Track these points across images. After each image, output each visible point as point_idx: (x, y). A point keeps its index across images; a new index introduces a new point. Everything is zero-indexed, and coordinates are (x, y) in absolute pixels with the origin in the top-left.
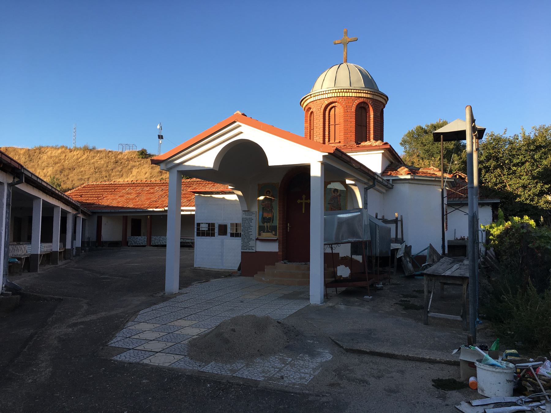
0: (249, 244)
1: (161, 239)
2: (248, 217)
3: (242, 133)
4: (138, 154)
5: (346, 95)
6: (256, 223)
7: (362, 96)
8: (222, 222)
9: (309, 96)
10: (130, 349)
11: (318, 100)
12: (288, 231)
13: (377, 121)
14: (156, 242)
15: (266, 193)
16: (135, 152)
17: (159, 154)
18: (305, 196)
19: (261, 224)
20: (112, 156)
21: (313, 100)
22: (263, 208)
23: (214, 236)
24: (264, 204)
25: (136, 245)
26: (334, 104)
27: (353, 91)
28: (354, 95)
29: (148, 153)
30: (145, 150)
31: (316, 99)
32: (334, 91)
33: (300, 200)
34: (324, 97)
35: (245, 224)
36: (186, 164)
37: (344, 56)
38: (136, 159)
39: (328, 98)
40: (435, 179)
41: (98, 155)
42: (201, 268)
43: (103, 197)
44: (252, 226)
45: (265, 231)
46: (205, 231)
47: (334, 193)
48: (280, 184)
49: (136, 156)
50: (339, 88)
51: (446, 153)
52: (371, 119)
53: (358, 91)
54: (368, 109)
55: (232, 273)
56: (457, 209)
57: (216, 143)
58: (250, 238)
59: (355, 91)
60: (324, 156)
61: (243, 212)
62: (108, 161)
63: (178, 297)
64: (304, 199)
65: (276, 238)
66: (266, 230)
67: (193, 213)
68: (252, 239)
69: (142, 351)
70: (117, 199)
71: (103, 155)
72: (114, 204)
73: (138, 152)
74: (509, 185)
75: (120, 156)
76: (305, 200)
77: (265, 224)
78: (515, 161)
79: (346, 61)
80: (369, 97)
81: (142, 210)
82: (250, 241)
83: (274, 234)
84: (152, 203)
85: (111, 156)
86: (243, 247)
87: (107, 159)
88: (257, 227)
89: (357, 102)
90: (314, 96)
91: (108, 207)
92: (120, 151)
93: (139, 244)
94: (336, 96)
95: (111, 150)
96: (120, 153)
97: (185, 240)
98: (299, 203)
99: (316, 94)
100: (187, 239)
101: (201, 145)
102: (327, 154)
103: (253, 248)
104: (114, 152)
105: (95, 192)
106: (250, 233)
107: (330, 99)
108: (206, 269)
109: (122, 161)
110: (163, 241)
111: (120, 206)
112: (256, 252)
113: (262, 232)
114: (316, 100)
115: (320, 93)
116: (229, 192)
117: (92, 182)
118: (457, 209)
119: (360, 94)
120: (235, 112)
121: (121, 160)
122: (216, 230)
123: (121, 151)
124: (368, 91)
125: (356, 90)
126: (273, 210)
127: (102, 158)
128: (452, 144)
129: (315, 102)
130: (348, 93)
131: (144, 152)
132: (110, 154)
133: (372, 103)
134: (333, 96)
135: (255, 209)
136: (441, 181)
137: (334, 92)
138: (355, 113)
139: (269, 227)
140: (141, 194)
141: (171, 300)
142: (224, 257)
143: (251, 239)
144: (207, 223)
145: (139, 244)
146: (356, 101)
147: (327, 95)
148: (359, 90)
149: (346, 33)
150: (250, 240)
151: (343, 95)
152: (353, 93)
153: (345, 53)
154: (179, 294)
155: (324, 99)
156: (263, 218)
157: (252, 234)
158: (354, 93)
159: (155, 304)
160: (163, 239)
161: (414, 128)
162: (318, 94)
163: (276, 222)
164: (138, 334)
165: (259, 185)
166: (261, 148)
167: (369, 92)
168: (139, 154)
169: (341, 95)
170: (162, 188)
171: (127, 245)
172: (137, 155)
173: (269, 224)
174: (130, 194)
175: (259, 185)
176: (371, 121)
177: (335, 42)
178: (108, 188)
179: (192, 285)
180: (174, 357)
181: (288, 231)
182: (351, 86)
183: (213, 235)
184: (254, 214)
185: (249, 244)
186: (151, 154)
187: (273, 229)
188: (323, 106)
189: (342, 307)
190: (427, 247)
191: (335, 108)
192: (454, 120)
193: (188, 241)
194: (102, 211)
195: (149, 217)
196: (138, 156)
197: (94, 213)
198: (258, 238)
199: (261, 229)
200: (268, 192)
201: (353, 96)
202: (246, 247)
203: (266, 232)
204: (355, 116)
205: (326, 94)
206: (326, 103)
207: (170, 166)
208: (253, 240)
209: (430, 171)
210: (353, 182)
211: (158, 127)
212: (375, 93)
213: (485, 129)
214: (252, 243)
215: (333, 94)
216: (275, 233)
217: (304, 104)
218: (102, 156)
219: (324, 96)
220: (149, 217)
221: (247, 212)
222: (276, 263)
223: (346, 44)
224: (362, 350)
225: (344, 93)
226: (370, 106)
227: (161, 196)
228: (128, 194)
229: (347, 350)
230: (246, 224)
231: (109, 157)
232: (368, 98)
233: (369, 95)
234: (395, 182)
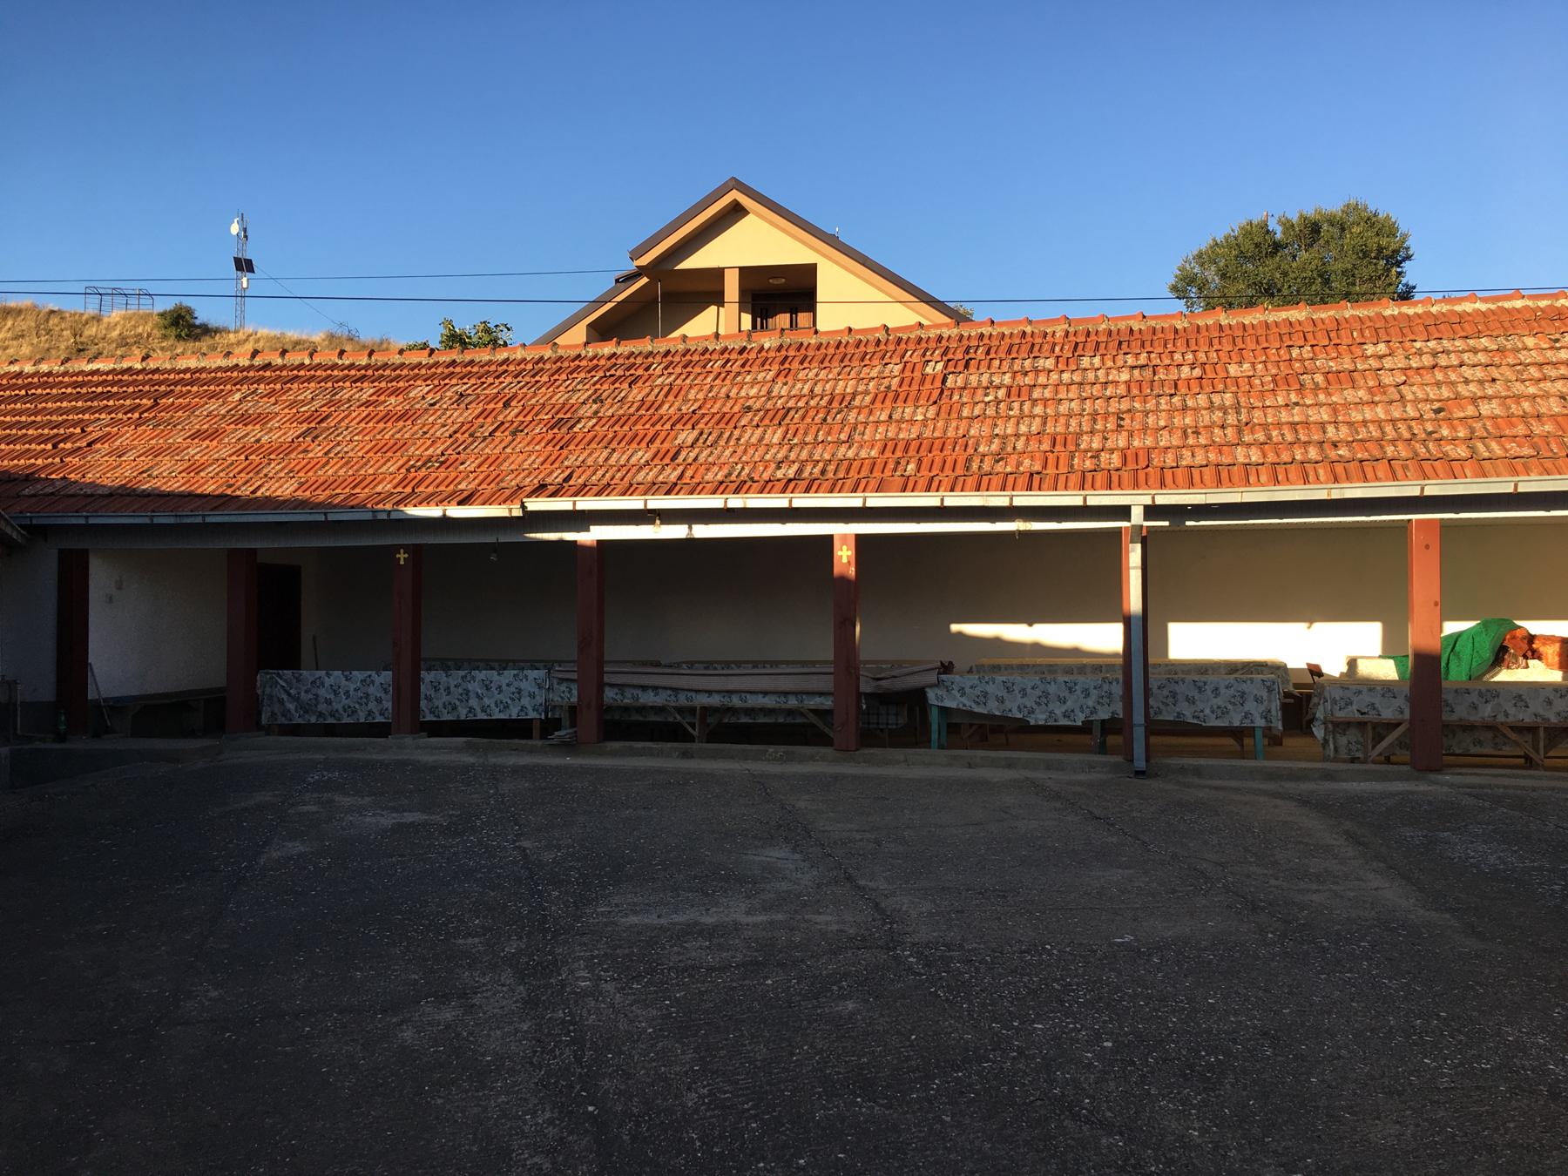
1: (475, 687)
4: (162, 322)
14: (439, 703)
16: (151, 315)
17: (238, 324)
20: (62, 330)
25: (313, 720)
29: (198, 322)
30: (190, 311)
38: (156, 341)
41: (9, 323)
43: (90, 438)
49: (155, 331)
62: (47, 346)
70: (179, 450)
71: (23, 324)
72: (168, 477)
73: (162, 315)
75: (94, 329)
81: (369, 516)
84: (423, 472)
85: (57, 329)
87: (43, 339)
91: (125, 496)
92: (92, 310)
93: (305, 708)
95: (56, 309)
96: (93, 318)
100: (644, 688)
104: (68, 315)
105: (36, 414)
109: (100, 345)
110: (486, 701)
111: (209, 488)
117: (11, 363)
121: (96, 344)
123: (97, 312)
127: (23, 336)
131: (184, 317)
132: (54, 321)
140: (331, 422)
145: (332, 715)
161: (1233, 231)
168: (166, 323)
170: (462, 389)
171: (258, 726)
172: (156, 326)
174: (261, 419)
178: (115, 389)
186: (210, 326)
193: (649, 699)
194: (91, 521)
195: (402, 556)
196: (163, 332)
197: (39, 532)
211: (235, 229)
218: (24, 327)
220: (402, 556)
227: (469, 429)
228: (245, 420)
231: (51, 330)
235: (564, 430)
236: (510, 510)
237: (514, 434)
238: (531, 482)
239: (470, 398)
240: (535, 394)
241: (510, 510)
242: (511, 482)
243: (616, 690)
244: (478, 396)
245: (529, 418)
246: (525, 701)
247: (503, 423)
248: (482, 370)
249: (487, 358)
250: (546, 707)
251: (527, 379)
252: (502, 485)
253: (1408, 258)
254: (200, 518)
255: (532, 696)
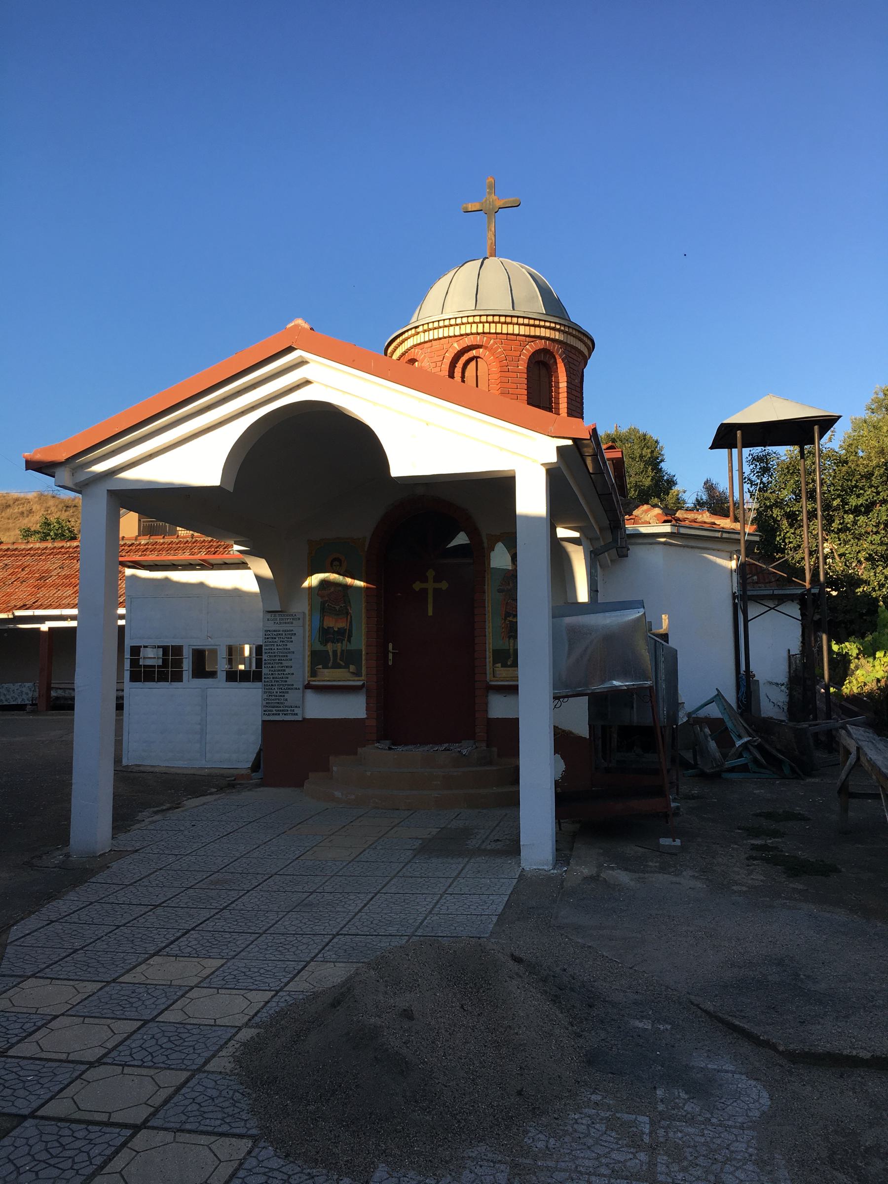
2: (281, 629)
3: (308, 382)
5: (505, 331)
6: (304, 643)
7: (543, 334)
8: (198, 644)
9: (413, 331)
10: (24, 1118)
11: (436, 340)
12: (390, 663)
13: (574, 398)
18: (434, 573)
19: (319, 647)
21: (422, 341)
22: (323, 604)
26: (474, 351)
27: (521, 321)
28: (523, 330)
31: (431, 338)
32: (477, 319)
34: (451, 334)
36: (125, 475)
37: (489, 242)
39: (462, 337)
40: (722, 535)
42: (142, 769)
46: (154, 666)
48: (367, 544)
50: (488, 313)
51: (638, 495)
52: (561, 391)
53: (532, 321)
54: (555, 367)
55: (235, 780)
56: (773, 608)
57: (180, 435)
58: (288, 685)
59: (526, 321)
60: (560, 450)
61: (269, 616)
63: (115, 866)
65: (360, 683)
66: (331, 661)
67: (74, 624)
69: (73, 1126)
74: (839, 555)
77: (330, 647)
78: (853, 501)
79: (493, 254)
80: (557, 337)
82: (288, 693)
83: (353, 673)
86: (267, 707)
88: (307, 653)
89: (530, 348)
90: (425, 331)
94: (480, 330)
97: (67, 691)
99: (431, 326)
101: (185, 414)
102: (569, 442)
103: (296, 710)
106: (288, 671)
107: (466, 339)
108: (157, 770)
110: (8, 697)
112: (304, 719)
113: (320, 666)
114: (430, 341)
115: (441, 324)
116: (221, 562)
118: (771, 609)
119: (538, 329)
120: (291, 322)
122: (187, 665)
124: (555, 323)
125: (529, 318)
128: (648, 476)
129: (426, 345)
130: (511, 326)
133: (564, 353)
134: (474, 331)
135: (301, 607)
136: (739, 540)
137: (476, 321)
138: (525, 376)
141: (99, 878)
142: (207, 736)
143: (291, 687)
144: (159, 647)
146: (527, 346)
147: (457, 328)
148: (535, 319)
149: (493, 187)
151: (499, 331)
152: (522, 327)
153: (490, 235)
154: (117, 854)
155: (451, 337)
157: (293, 674)
158: (524, 327)
159: (51, 897)
160: (9, 691)
162: (436, 325)
163: (360, 641)
164: (30, 1034)
166: (368, 426)
167: (558, 327)
169: (493, 331)
170: (6, 562)
176: (561, 396)
177: (467, 208)
179: (139, 822)
180: (213, 1147)
181: (390, 663)
182: (514, 309)
183: (177, 677)
185: (286, 700)
187: (349, 659)
188: (449, 356)
189: (623, 877)
190: (713, 698)
191: (477, 361)
192: (760, 398)
199: (318, 659)
201: (521, 333)
202: (285, 711)
203: (332, 668)
204: (526, 382)
205: (457, 325)
206: (457, 347)
207: (81, 477)
208: (296, 689)
209: (703, 516)
210: (576, 535)
212: (571, 330)
213: (711, 448)
214: (292, 697)
215: (474, 326)
217: (395, 350)
219: (451, 331)
222: (360, 750)
223: (491, 212)
224: (845, 1053)
225: (499, 326)
226: (559, 361)
229: (793, 1057)
232: (554, 340)
233: (557, 333)
234: (633, 541)
235: (42, 581)
236: (8, 615)
237: (22, 583)
238: (20, 604)
239: (9, 566)
240: (37, 565)
241: (8, 615)
242: (12, 604)
243: (62, 691)
244: (13, 565)
245: (30, 576)
246: (24, 696)
247: (19, 578)
248: (19, 553)
249: (24, 547)
250: (33, 698)
251: (36, 557)
252: (9, 605)
253: (662, 461)
254: (772, 591)
255: (27, 694)
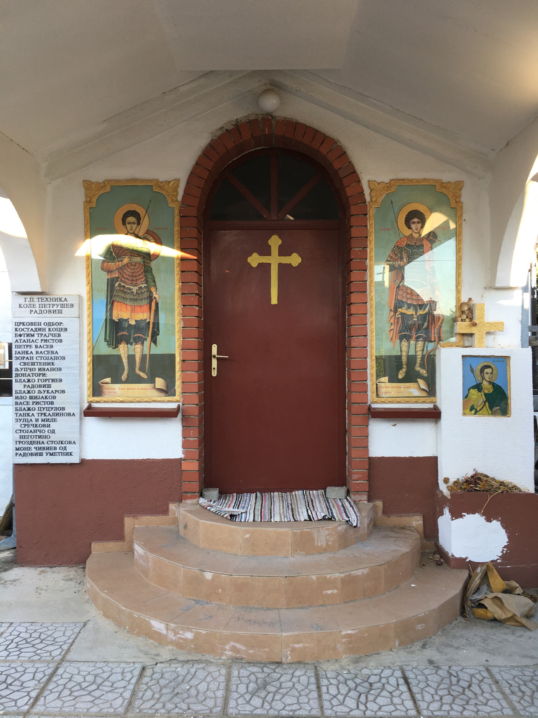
0: (53, 432)
2: (43, 321)
12: (214, 373)
15: (124, 222)
19: (105, 349)
22: (111, 283)
23: (270, 255)
24: (113, 265)
33: (261, 254)
35: (28, 349)
44: (64, 358)
45: (124, 377)
47: (410, 228)
58: (56, 409)
61: (21, 299)
64: (275, 250)
65: (174, 406)
66: (126, 372)
68: (67, 411)
76: (280, 254)
77: (123, 350)
82: (55, 420)
88: (87, 359)
98: (254, 265)
103: (70, 448)
106: (55, 386)
113: (108, 380)
126: (153, 290)
139: (138, 360)
143: (60, 412)
150: (57, 414)
156: (112, 321)
157: (63, 392)
165: (88, 185)
173: (138, 347)
175: (88, 185)
181: (214, 373)
184: (72, 306)
198: (90, 405)
200: (131, 219)
202: (38, 443)
203: (127, 382)
208: (69, 414)
216: (167, 386)
221: (35, 297)
222: (172, 507)
230: (34, 350)
